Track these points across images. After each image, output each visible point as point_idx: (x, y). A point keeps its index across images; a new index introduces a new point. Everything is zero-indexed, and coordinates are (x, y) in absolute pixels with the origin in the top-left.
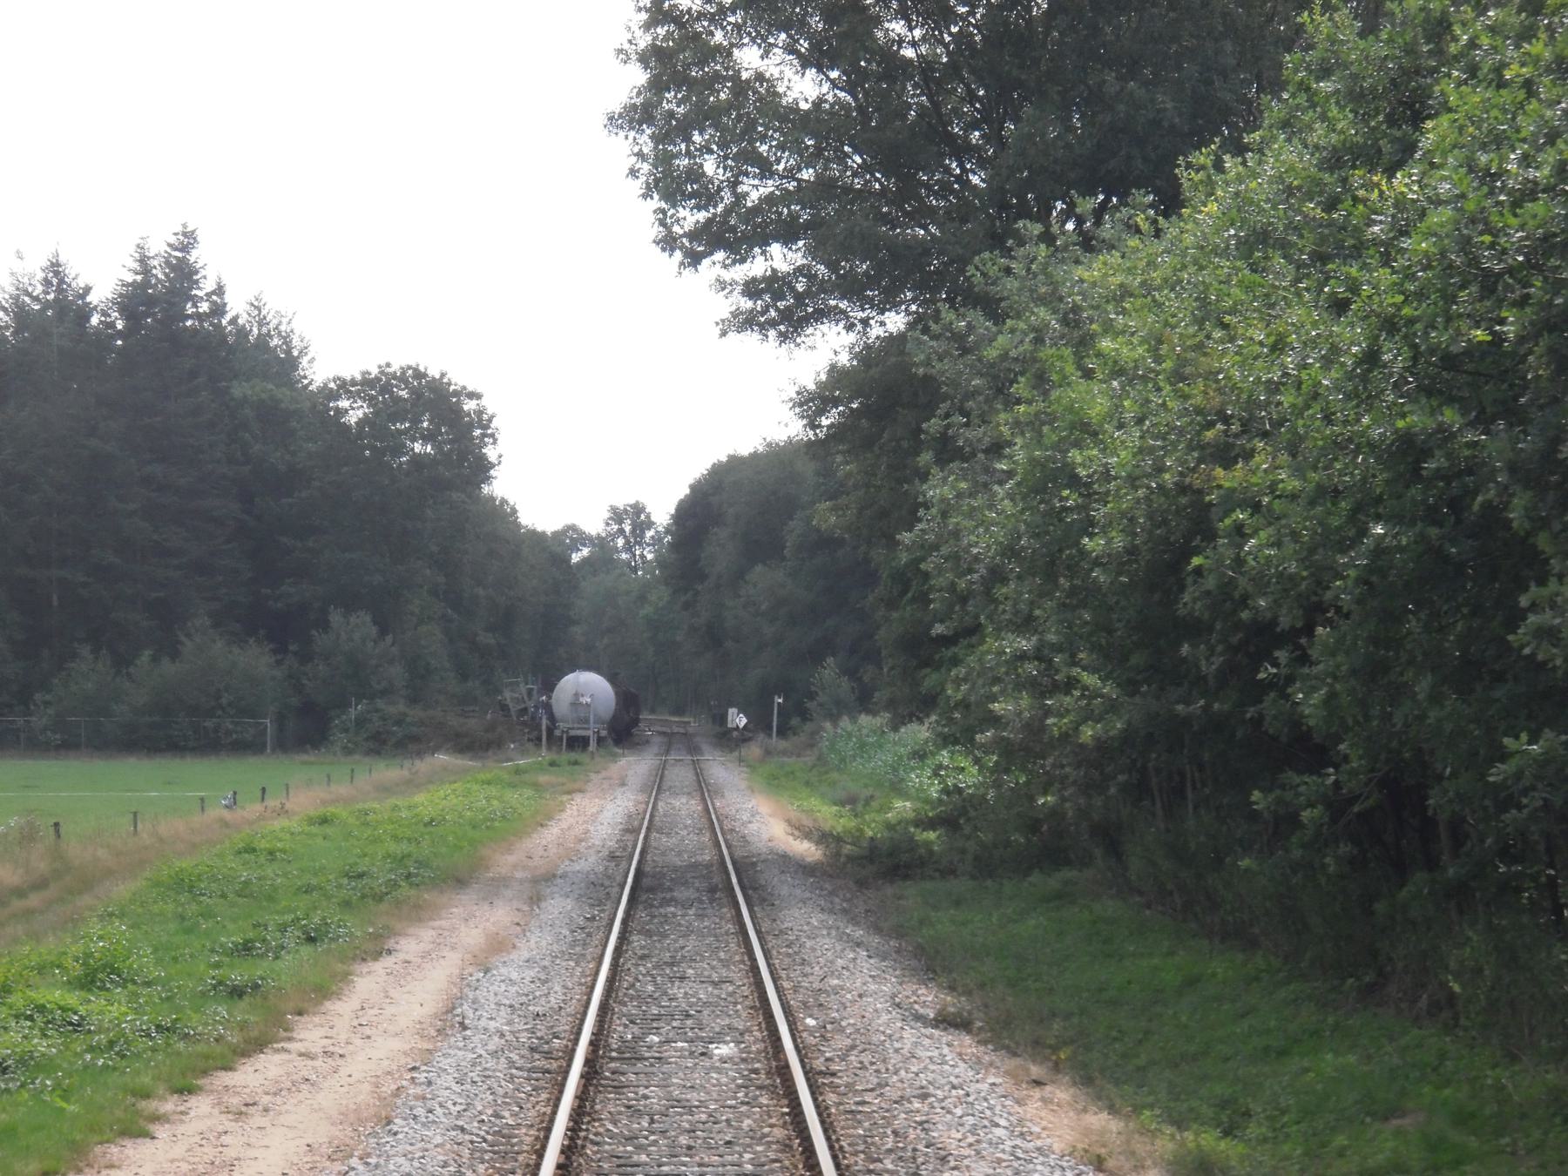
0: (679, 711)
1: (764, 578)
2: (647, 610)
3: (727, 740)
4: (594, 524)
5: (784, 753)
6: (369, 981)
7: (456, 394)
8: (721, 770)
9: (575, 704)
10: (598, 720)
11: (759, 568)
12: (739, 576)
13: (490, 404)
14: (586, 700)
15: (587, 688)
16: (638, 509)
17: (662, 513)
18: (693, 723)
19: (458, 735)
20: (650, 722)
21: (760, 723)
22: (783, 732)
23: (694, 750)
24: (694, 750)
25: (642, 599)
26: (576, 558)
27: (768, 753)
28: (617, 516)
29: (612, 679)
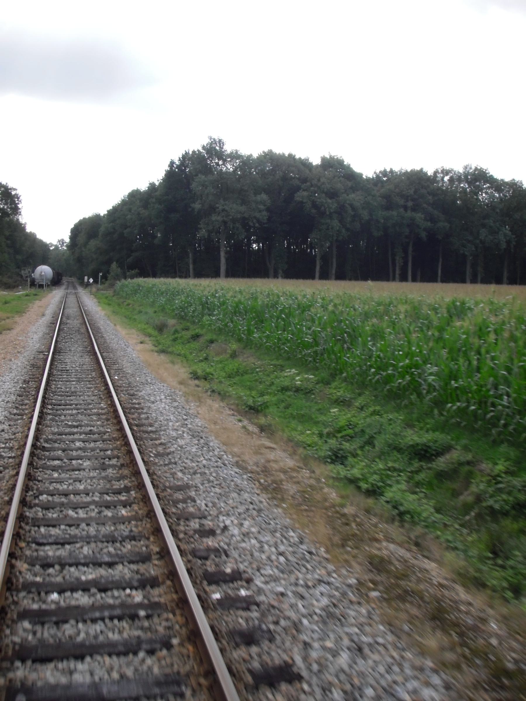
0: (71, 277)
1: (93, 243)
2: (64, 257)
3: (87, 285)
4: (55, 242)
5: (102, 290)
6: (21, 321)
7: (10, 189)
8: (82, 292)
9: (41, 275)
10: (47, 279)
11: (92, 241)
12: (86, 244)
13: (19, 192)
14: (43, 273)
15: (44, 271)
16: (63, 240)
17: (67, 240)
18: (73, 279)
19: (6, 284)
20: (65, 280)
21: (96, 281)
22: (102, 283)
23: (75, 288)
24: (75, 288)
25: (63, 255)
26: (51, 248)
27: (98, 290)
28: (59, 241)
29: (53, 269)
